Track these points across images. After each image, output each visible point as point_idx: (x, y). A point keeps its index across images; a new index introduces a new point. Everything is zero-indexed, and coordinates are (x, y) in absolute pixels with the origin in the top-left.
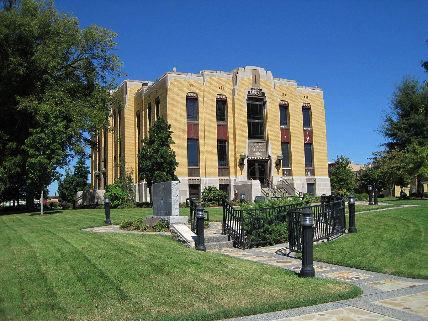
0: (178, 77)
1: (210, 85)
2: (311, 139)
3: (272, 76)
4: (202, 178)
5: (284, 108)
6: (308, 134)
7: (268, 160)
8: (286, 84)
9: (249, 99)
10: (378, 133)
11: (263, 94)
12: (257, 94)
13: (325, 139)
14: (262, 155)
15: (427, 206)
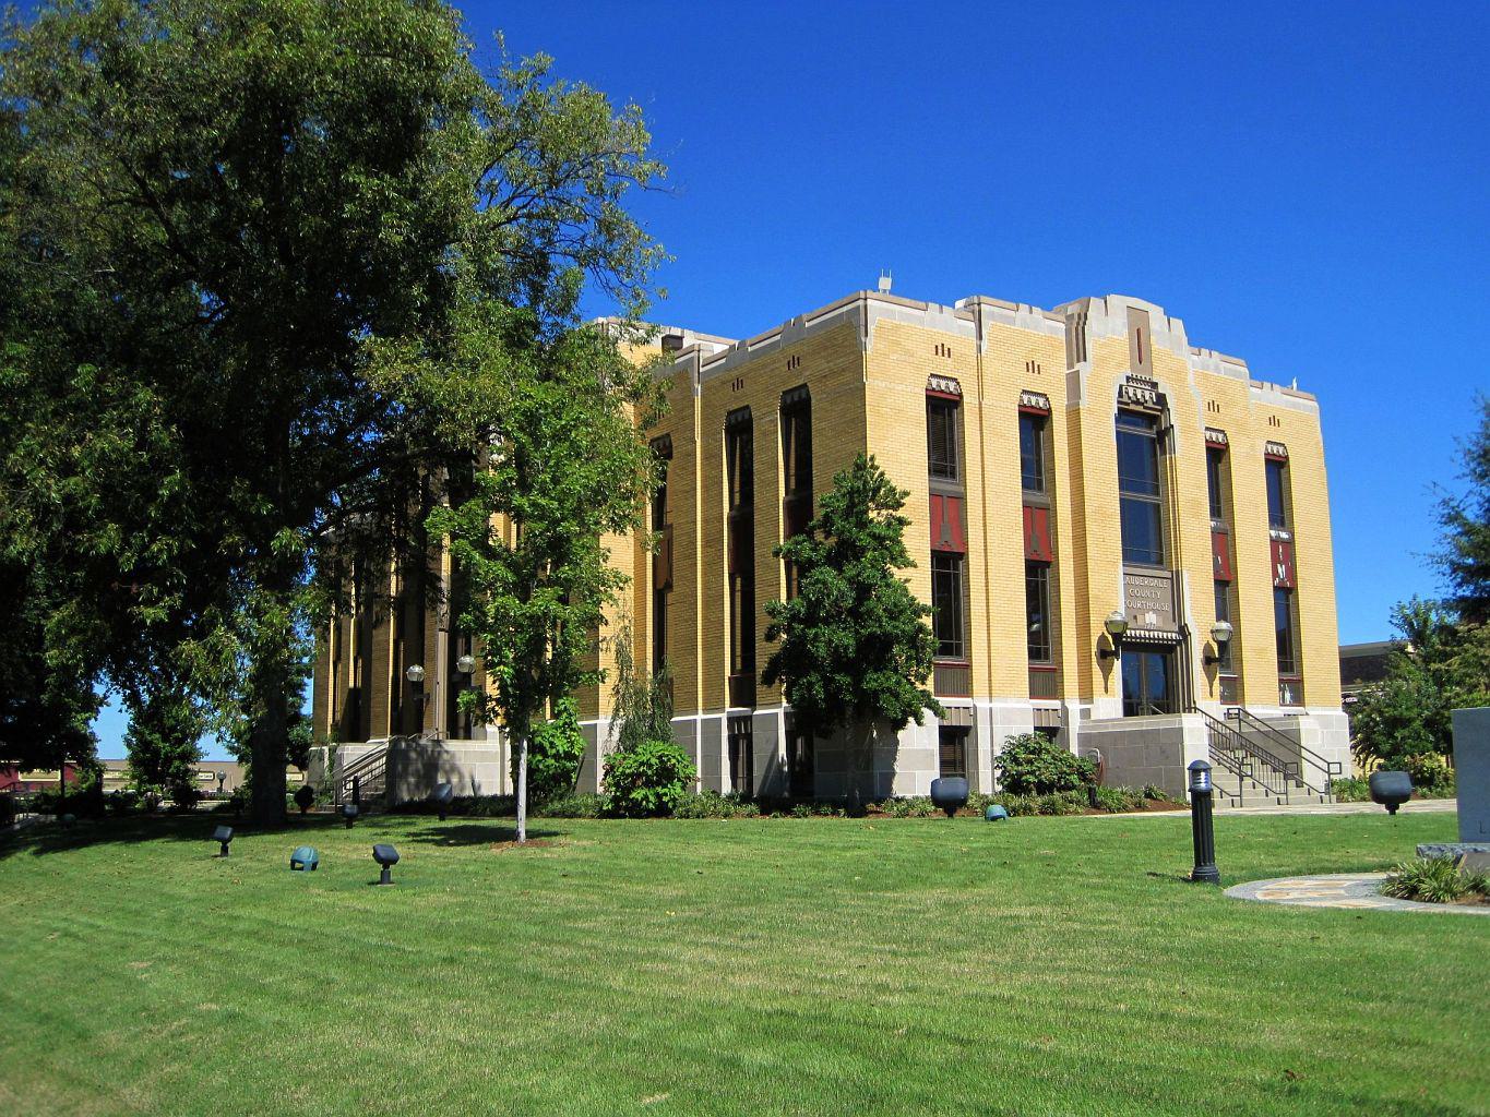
0: (900, 312)
1: (1003, 351)
2: (1292, 572)
3: (1185, 339)
4: (980, 701)
5: (1217, 454)
6: (1283, 552)
7: (1179, 642)
8: (1217, 369)
9: (1124, 415)
10: (1425, 562)
11: (1161, 399)
12: (1142, 400)
13: (1330, 576)
14: (1161, 624)
15: (1186, 818)
